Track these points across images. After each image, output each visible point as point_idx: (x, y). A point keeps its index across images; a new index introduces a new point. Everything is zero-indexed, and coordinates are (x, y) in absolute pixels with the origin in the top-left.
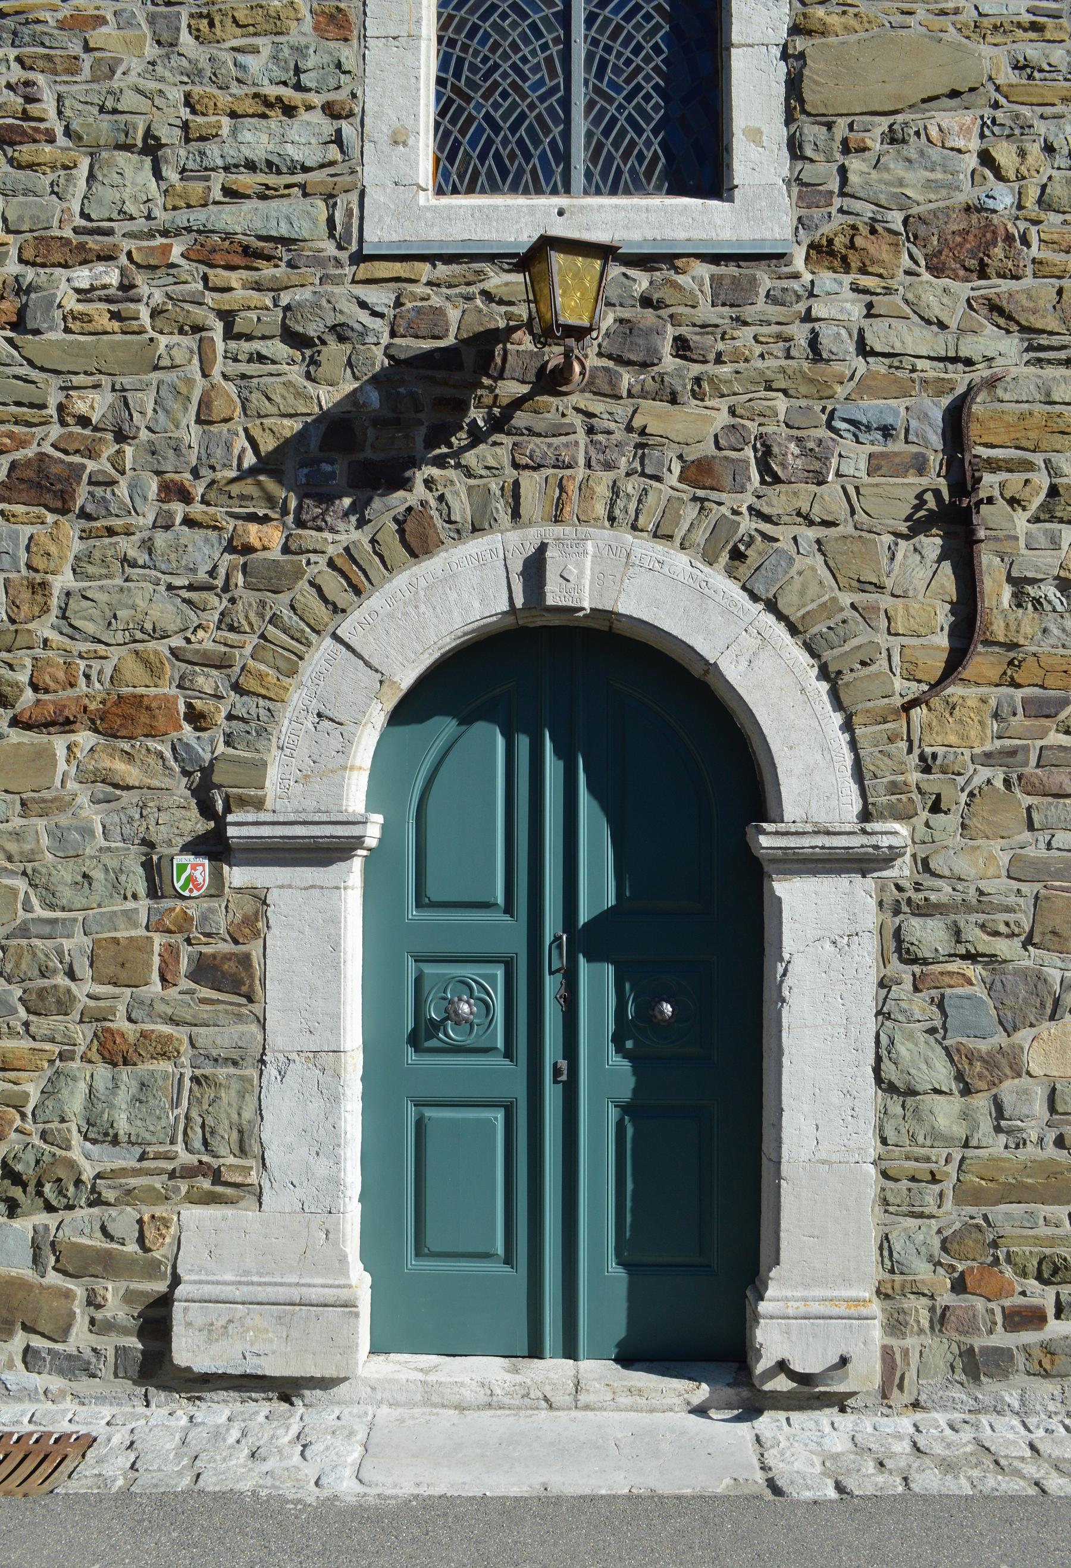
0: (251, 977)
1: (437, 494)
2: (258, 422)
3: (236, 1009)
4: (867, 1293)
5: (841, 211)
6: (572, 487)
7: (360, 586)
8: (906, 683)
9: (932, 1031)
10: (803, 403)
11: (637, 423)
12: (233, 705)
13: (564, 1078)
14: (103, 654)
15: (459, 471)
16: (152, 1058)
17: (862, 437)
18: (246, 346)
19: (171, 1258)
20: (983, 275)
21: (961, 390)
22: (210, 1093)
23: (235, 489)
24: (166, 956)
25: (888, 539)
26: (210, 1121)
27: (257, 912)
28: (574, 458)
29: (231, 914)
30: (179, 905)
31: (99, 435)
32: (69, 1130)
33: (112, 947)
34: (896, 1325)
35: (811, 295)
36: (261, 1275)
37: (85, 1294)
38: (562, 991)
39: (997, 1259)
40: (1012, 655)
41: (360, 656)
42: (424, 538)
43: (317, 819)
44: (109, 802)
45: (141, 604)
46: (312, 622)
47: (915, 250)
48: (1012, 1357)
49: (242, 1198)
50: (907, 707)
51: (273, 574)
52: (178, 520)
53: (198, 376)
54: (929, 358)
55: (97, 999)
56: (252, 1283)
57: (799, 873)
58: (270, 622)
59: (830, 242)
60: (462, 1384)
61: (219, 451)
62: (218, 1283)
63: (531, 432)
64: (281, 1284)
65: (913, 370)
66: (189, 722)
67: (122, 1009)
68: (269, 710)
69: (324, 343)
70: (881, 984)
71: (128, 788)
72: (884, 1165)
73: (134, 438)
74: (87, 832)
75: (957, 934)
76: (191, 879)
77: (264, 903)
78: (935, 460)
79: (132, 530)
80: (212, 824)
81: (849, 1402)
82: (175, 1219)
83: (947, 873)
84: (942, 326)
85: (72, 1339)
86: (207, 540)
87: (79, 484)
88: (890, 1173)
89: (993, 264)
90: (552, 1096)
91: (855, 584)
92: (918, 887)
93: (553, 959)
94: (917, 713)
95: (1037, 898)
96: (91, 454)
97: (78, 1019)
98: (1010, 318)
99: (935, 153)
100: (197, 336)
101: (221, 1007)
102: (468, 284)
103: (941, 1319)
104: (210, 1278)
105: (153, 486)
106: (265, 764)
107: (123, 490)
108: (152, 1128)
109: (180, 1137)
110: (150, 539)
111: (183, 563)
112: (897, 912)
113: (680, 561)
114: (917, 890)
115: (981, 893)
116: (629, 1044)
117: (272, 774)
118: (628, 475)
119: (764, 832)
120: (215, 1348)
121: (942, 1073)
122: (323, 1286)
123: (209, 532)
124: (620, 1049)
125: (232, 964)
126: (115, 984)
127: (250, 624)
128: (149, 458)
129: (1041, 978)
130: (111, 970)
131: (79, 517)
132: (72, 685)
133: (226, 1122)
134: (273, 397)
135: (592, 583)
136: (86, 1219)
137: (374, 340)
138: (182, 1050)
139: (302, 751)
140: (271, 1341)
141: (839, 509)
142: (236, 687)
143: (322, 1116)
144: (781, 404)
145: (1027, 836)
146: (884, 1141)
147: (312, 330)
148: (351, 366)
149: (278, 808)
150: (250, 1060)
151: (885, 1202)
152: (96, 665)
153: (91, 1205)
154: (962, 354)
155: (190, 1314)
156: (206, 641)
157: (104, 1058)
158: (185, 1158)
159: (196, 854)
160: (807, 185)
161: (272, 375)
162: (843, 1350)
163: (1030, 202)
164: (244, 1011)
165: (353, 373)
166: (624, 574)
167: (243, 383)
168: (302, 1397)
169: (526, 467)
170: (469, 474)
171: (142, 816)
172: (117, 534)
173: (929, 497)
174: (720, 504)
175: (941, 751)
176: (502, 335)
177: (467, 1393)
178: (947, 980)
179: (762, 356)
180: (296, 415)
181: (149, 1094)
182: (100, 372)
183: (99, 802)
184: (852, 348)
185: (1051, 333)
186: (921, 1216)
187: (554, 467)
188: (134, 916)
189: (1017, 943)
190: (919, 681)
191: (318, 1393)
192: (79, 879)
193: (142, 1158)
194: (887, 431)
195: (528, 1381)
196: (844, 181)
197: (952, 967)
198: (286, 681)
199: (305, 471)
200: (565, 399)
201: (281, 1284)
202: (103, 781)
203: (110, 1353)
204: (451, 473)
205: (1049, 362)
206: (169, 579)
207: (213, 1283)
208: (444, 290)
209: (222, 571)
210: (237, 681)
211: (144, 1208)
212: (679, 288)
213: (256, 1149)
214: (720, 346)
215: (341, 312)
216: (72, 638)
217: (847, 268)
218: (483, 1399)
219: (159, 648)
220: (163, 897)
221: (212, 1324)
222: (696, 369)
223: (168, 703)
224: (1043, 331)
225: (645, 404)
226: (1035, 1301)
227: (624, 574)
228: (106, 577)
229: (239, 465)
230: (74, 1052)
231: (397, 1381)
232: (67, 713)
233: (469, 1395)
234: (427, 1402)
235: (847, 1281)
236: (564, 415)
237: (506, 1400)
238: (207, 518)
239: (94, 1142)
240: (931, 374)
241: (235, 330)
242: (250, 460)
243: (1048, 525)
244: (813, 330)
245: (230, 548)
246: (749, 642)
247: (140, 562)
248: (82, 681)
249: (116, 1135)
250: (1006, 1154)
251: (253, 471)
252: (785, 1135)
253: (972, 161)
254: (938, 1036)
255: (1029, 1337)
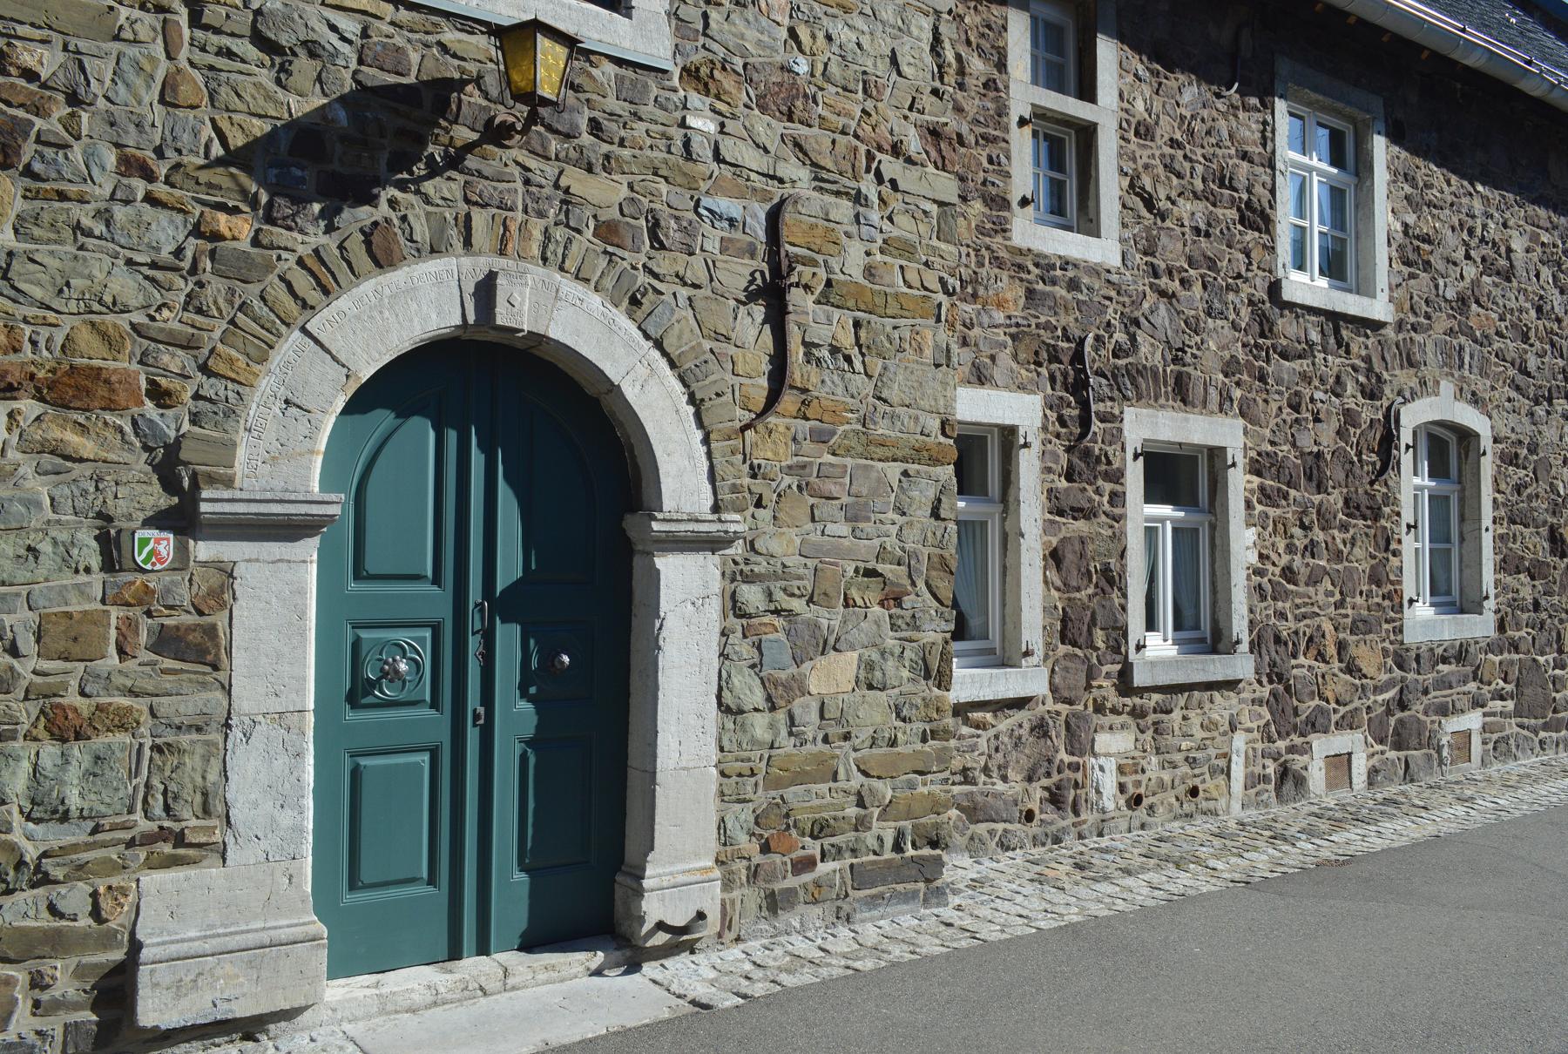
0: (217, 646)
1: (400, 214)
2: (226, 115)
3: (201, 678)
4: (710, 863)
5: (704, 46)
6: (513, 227)
7: (329, 287)
8: (742, 412)
9: (753, 666)
10: (678, 190)
11: (563, 182)
12: (201, 386)
13: (482, 722)
14: (53, 321)
15: (418, 197)
16: (108, 730)
17: (717, 224)
18: (215, 39)
19: (129, 927)
20: (790, 119)
21: (776, 200)
22: (173, 760)
23: (204, 176)
24: (124, 629)
25: (732, 303)
26: (173, 787)
27: (223, 584)
28: (514, 202)
29: (195, 587)
30: (139, 578)
31: (48, 93)
32: (9, 813)
33: (64, 622)
34: (728, 884)
35: (685, 107)
36: (226, 926)
37: (28, 978)
38: (481, 649)
39: (788, 826)
40: (804, 397)
41: (328, 351)
42: (389, 252)
43: (293, 498)
44: (58, 473)
45: (99, 276)
46: (282, 315)
47: (750, 89)
48: (797, 893)
49: (205, 857)
50: (743, 429)
51: (243, 265)
52: (140, 196)
53: (163, 56)
54: (757, 172)
55: (45, 674)
56: (219, 935)
57: (672, 550)
58: (240, 309)
59: (697, 69)
60: (413, 990)
61: (185, 136)
62: (183, 941)
63: (480, 175)
64: (248, 931)
65: (748, 180)
66: (151, 398)
67: (74, 684)
68: (238, 393)
69: (295, 54)
70: (723, 634)
71: (81, 460)
72: (722, 766)
73: (90, 104)
74: (32, 504)
75: (770, 596)
76: (153, 552)
77: (231, 575)
78: (761, 249)
79: (87, 198)
80: (176, 500)
81: (698, 945)
82: (134, 886)
83: (765, 552)
84: (766, 151)
85: (11, 1027)
86: (171, 221)
87: (25, 140)
88: (727, 772)
89: (797, 113)
90: (472, 736)
91: (713, 334)
92: (747, 561)
93: (475, 622)
94: (748, 433)
95: (816, 570)
96: (39, 111)
97: (22, 695)
98: (806, 154)
99: (764, 21)
100: (161, 17)
101: (185, 676)
102: (427, 33)
103: (754, 874)
104: (173, 938)
105: (111, 158)
106: (234, 445)
107: (77, 154)
108: (108, 800)
109: (139, 806)
110: (107, 210)
111: (146, 240)
112: (733, 580)
113: (595, 300)
114: (747, 564)
115: (784, 566)
116: (533, 690)
117: (241, 453)
118: (556, 224)
119: (656, 519)
120: (184, 1003)
121: (757, 697)
122: (288, 926)
123: (174, 213)
124: (524, 694)
125: (196, 634)
126: (66, 659)
127: (219, 309)
128: (108, 128)
129: (817, 626)
130: (61, 645)
131: (22, 174)
132: (15, 350)
133: (190, 786)
134: (243, 94)
135: (529, 310)
136: (29, 901)
137: (344, 63)
138: (142, 720)
139: (270, 436)
140: (242, 985)
141: (702, 277)
142: (204, 369)
143: (287, 771)
144: (663, 187)
145: (810, 526)
146: (722, 749)
147: (285, 39)
148: (321, 83)
149: (245, 486)
150: (214, 725)
151: (722, 794)
152: (45, 332)
153: (33, 886)
154: (779, 174)
155: (157, 975)
156: (170, 320)
157: (52, 734)
158: (144, 825)
159: (161, 528)
160: (682, 21)
161: (241, 73)
162: (698, 907)
163: (818, 73)
164: (209, 679)
165: (322, 88)
166: (553, 306)
167: (210, 74)
168: (267, 1032)
169: (476, 204)
170: (427, 200)
171: (97, 488)
172: (69, 200)
173: (757, 275)
174: (623, 259)
175: (763, 462)
176: (460, 85)
177: (416, 997)
178: (763, 628)
179: (651, 147)
180: (266, 116)
181: (106, 766)
182: (50, 28)
183: (46, 473)
184: (710, 154)
185: (829, 171)
186: (745, 801)
187: (498, 208)
188: (88, 590)
189: (803, 601)
190: (750, 411)
191: (283, 1024)
192: (23, 552)
193: (95, 831)
194: (732, 222)
195: (467, 976)
196: (706, 25)
197: (766, 620)
198: (256, 368)
199: (275, 171)
200: (507, 151)
201: (248, 931)
202: (52, 453)
203: (59, 1034)
204: (411, 197)
205: (827, 191)
206: (129, 254)
207: (178, 941)
208: (406, 33)
209: (189, 254)
210: (205, 363)
211: (97, 881)
212: (590, 76)
213: (220, 808)
214: (623, 133)
215: (313, 29)
216: (15, 301)
217: (707, 94)
218: (429, 999)
219: (119, 322)
220: (121, 570)
221: (181, 980)
222: (605, 148)
223: (128, 379)
224: (823, 168)
225: (569, 169)
226: (808, 852)
227: (553, 306)
228: (56, 242)
229: (207, 155)
230: (16, 731)
231: (356, 999)
232: (9, 379)
233: (417, 998)
234: (383, 1011)
235: (697, 856)
236: (506, 165)
237: (449, 996)
238: (172, 200)
239: (38, 821)
240: (758, 185)
241: (204, 21)
242: (217, 150)
243: (825, 307)
244: (686, 135)
245: (196, 232)
246: (642, 371)
247: (97, 233)
248: (27, 347)
249: (67, 811)
250: (795, 751)
251: (219, 162)
252: (659, 751)
253: (784, 34)
254: (757, 670)
255: (807, 877)
